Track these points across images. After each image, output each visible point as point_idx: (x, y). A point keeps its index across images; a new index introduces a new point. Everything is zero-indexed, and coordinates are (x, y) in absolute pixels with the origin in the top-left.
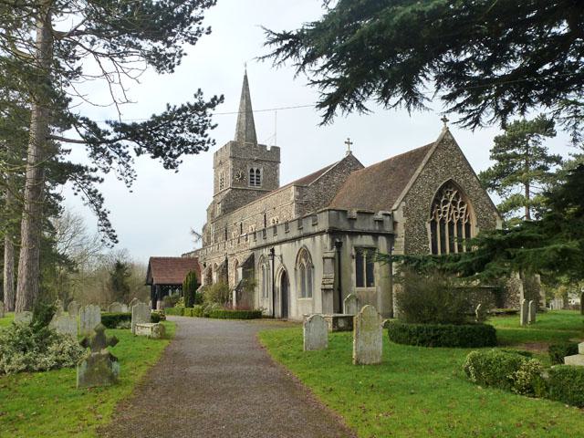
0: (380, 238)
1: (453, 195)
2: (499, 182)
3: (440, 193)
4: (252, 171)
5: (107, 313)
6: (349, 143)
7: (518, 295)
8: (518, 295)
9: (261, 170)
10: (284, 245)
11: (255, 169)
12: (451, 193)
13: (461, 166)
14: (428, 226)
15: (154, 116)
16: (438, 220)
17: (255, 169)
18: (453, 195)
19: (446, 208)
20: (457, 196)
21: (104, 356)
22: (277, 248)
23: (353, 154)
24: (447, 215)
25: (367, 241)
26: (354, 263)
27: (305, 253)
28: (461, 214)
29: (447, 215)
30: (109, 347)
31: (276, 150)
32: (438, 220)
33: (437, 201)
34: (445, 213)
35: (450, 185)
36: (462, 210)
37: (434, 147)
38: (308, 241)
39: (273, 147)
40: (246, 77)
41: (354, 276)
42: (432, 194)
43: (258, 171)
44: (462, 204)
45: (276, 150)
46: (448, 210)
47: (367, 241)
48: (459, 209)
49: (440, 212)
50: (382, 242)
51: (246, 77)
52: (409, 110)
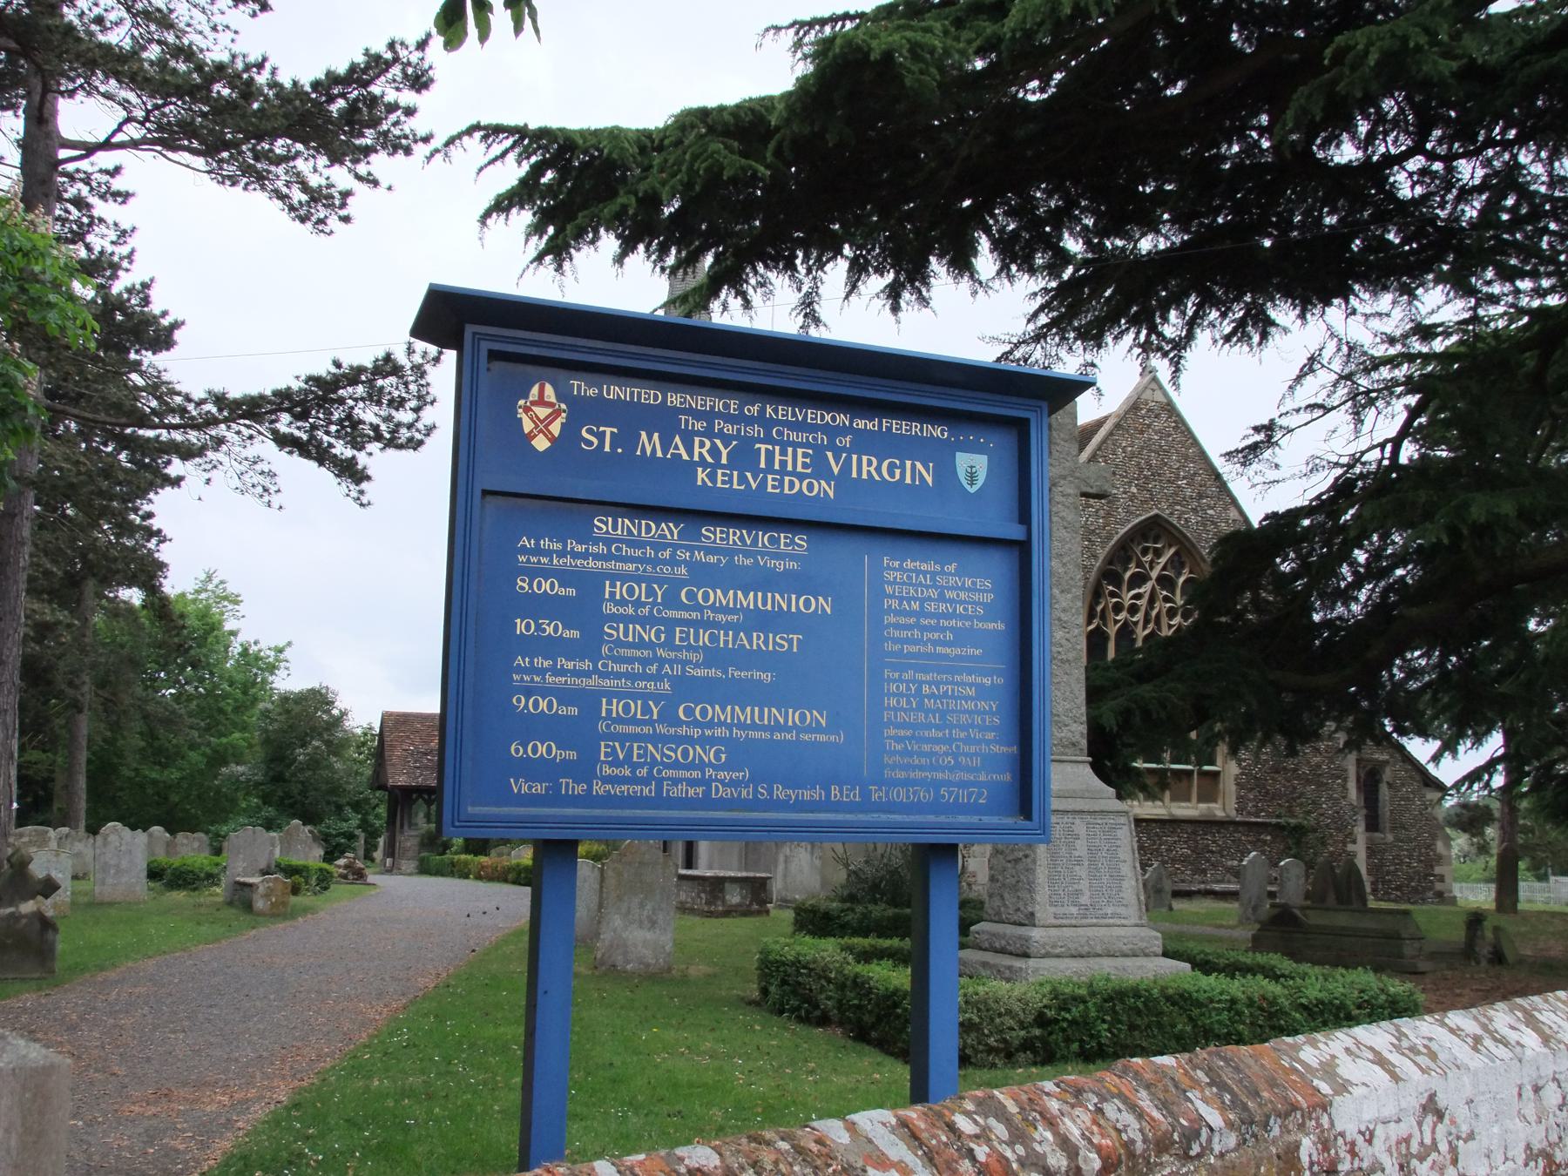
1: (1163, 560)
2: (211, 408)
3: (1122, 554)
5: (161, 858)
6: (390, 188)
7: (1350, 847)
8: (1350, 847)
12: (1158, 553)
13: (1191, 478)
15: (329, 74)
18: (1163, 560)
19: (1138, 597)
21: (25, 916)
24: (1139, 617)
29: (1139, 617)
30: (40, 898)
32: (1112, 630)
33: (1110, 575)
36: (1138, 597)
42: (1095, 557)
46: (1143, 603)
49: (1118, 608)
52: (527, 241)
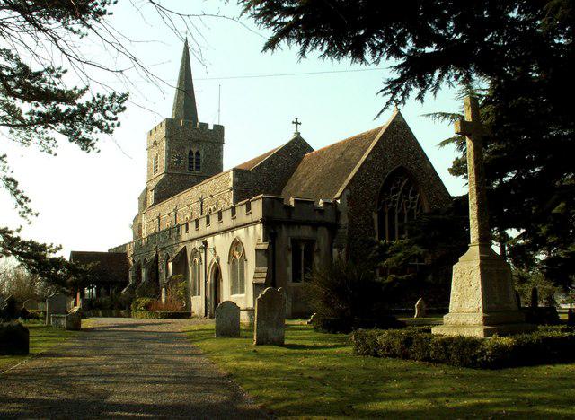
0: (319, 229)
1: (404, 184)
4: (191, 153)
6: (297, 123)
9: (202, 153)
10: (218, 237)
11: (194, 152)
12: (402, 181)
14: (375, 217)
16: (387, 211)
17: (194, 152)
19: (415, 199)
20: (409, 185)
22: (209, 240)
23: (302, 136)
24: (396, 205)
25: (306, 232)
26: (290, 257)
27: (236, 244)
28: (413, 204)
29: (396, 205)
34: (394, 202)
35: (401, 172)
37: (383, 130)
38: (240, 233)
41: (290, 270)
43: (198, 153)
44: (414, 193)
47: (306, 232)
48: (411, 199)
50: (322, 237)
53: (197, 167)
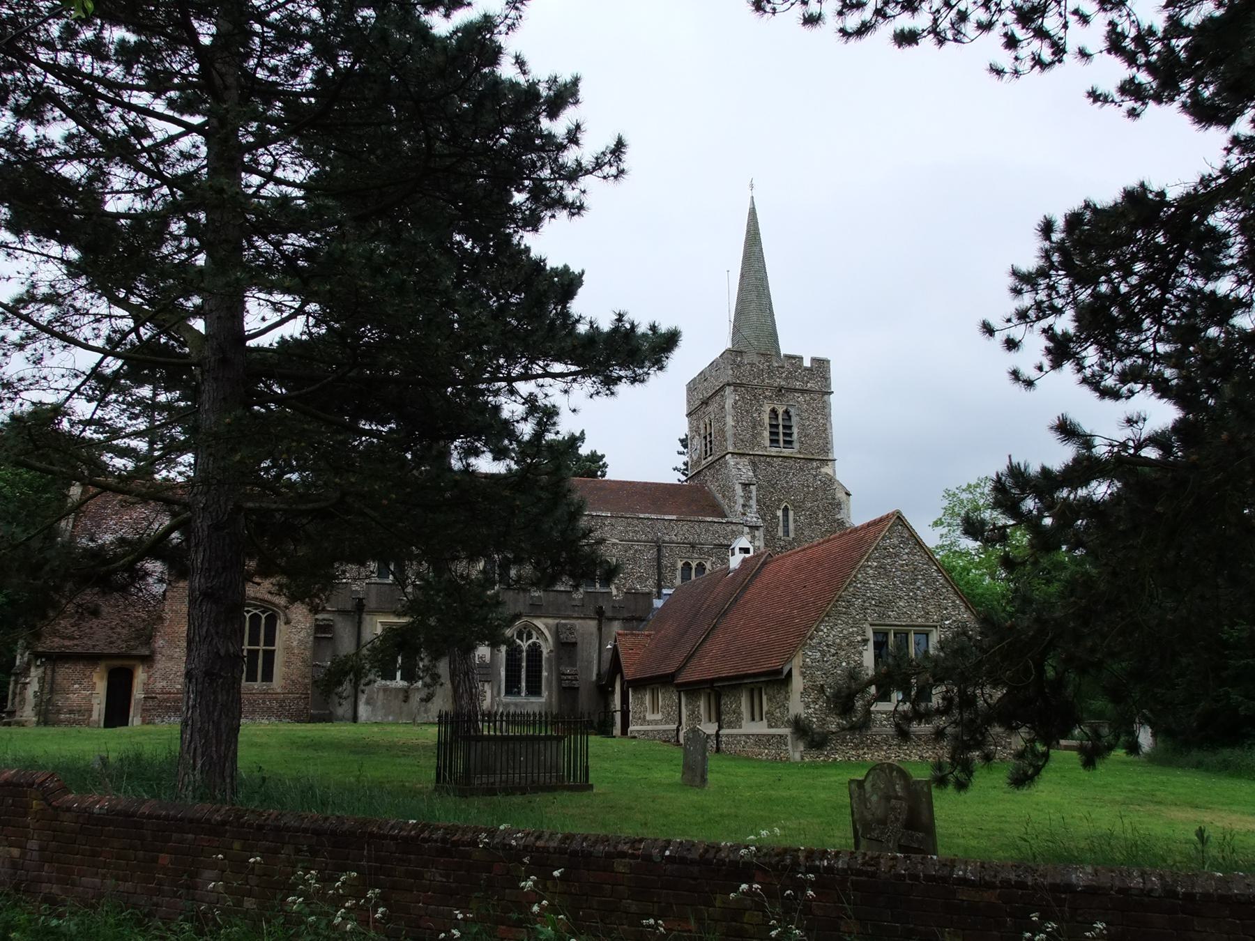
17: (781, 411)
31: (821, 366)
39: (814, 360)
40: (753, 213)
45: (821, 366)
51: (753, 213)
53: (785, 442)
